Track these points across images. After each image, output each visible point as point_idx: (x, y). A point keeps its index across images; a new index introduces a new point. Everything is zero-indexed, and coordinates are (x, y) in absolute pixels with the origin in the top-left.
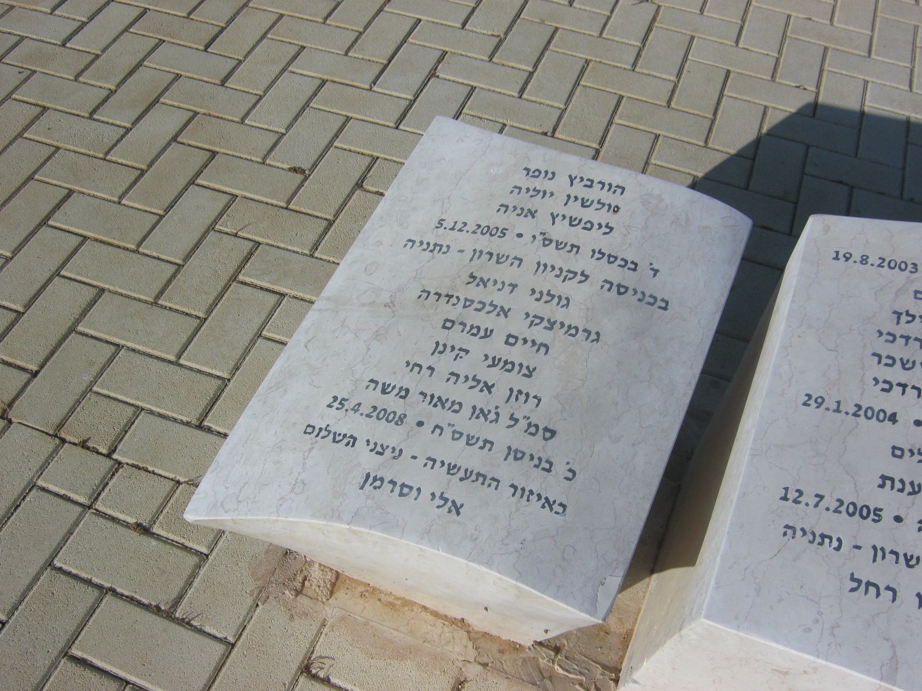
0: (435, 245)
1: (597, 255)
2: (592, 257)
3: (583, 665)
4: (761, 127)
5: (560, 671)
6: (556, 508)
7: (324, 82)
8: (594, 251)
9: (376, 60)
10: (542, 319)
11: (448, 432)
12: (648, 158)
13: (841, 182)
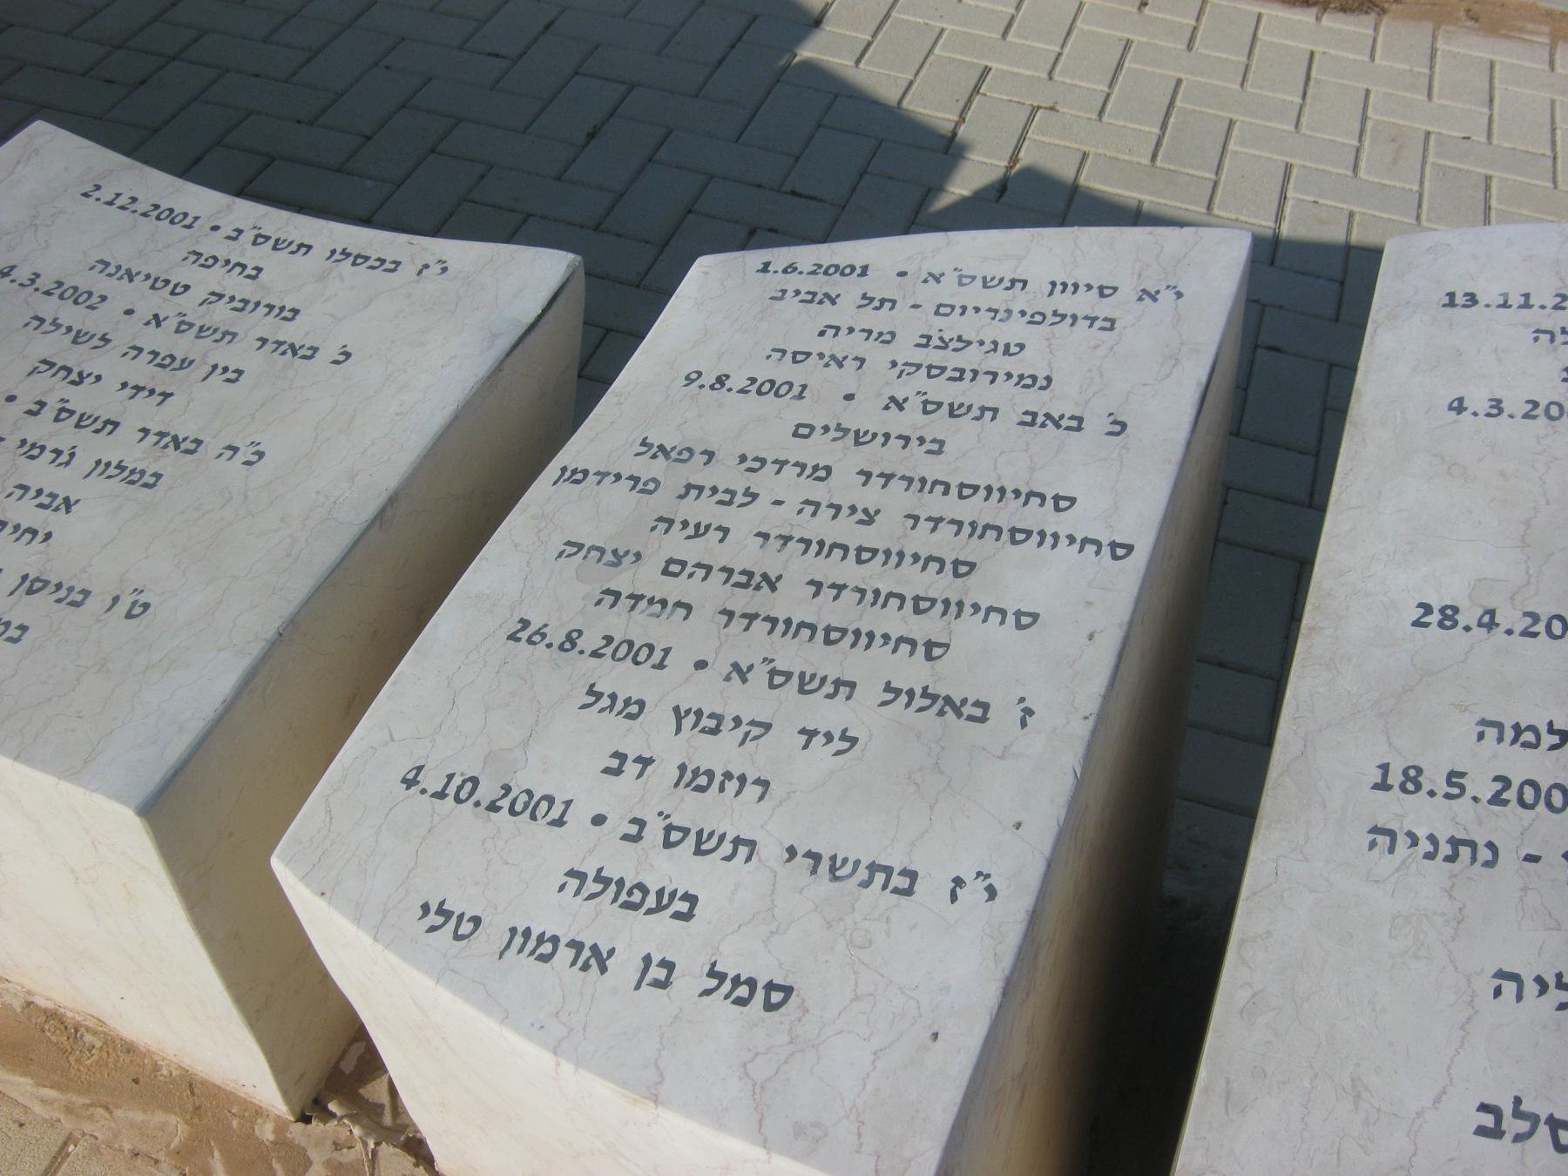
1: (337, 256)
11: (759, 676)
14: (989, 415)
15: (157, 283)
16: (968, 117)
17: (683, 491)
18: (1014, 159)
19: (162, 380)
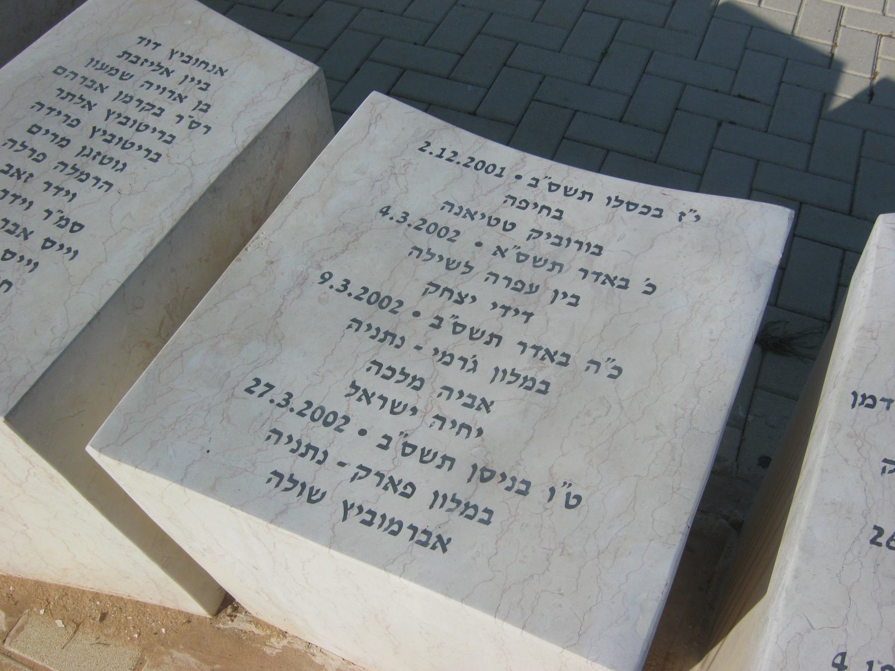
1: (613, 203)
2: (608, 204)
8: (609, 199)
14: (587, 197)
15: (492, 221)
16: (839, 41)
17: (121, 54)
18: (874, 74)
19: (521, 301)
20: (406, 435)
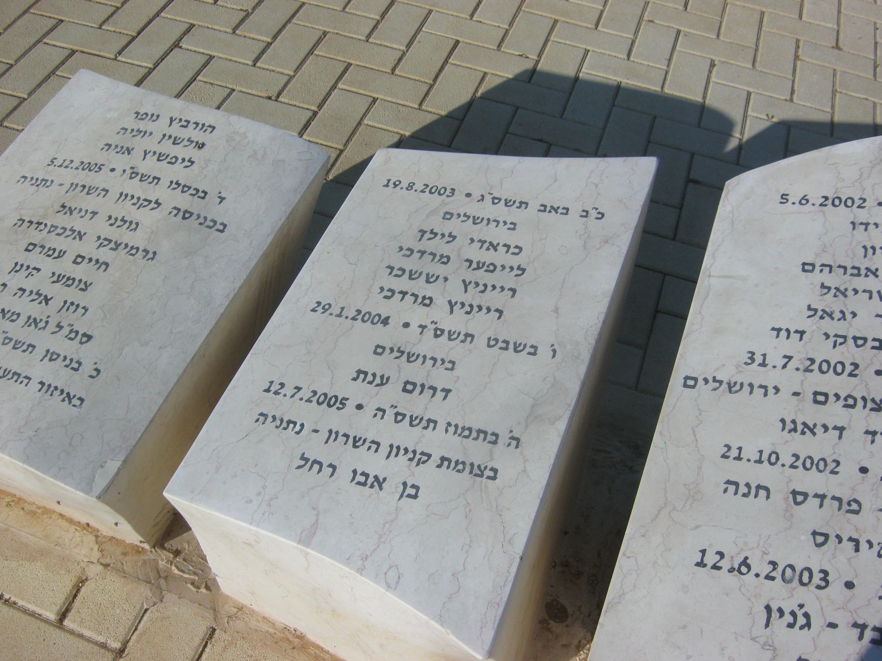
0: (43, 180)
1: (174, 186)
3: (199, 566)
4: (476, 90)
5: (176, 571)
6: (75, 401)
7: (73, 52)
9: (126, 32)
10: (110, 241)
12: (362, 119)
13: (541, 140)
14: (524, 206)
20: (436, 323)
